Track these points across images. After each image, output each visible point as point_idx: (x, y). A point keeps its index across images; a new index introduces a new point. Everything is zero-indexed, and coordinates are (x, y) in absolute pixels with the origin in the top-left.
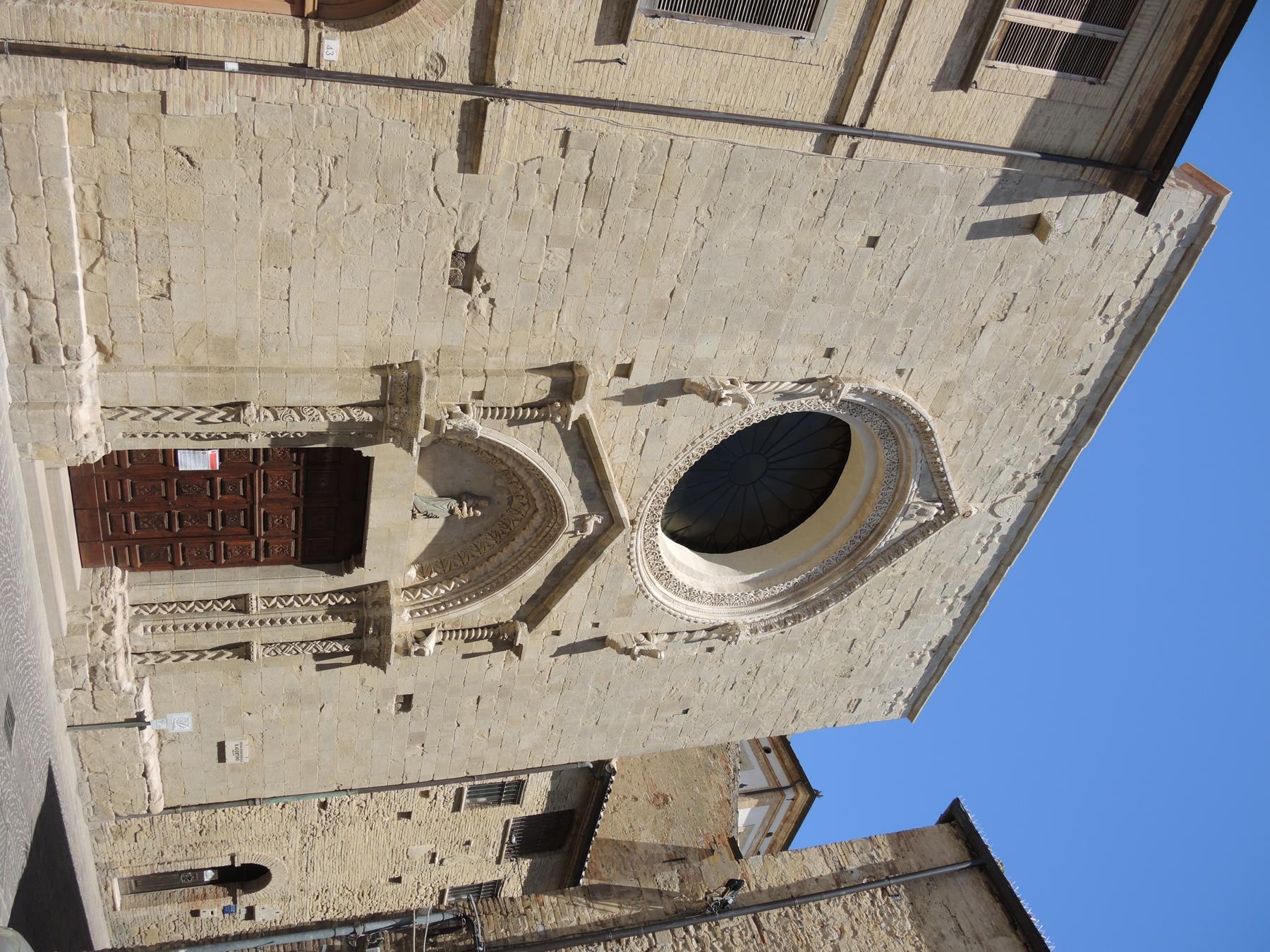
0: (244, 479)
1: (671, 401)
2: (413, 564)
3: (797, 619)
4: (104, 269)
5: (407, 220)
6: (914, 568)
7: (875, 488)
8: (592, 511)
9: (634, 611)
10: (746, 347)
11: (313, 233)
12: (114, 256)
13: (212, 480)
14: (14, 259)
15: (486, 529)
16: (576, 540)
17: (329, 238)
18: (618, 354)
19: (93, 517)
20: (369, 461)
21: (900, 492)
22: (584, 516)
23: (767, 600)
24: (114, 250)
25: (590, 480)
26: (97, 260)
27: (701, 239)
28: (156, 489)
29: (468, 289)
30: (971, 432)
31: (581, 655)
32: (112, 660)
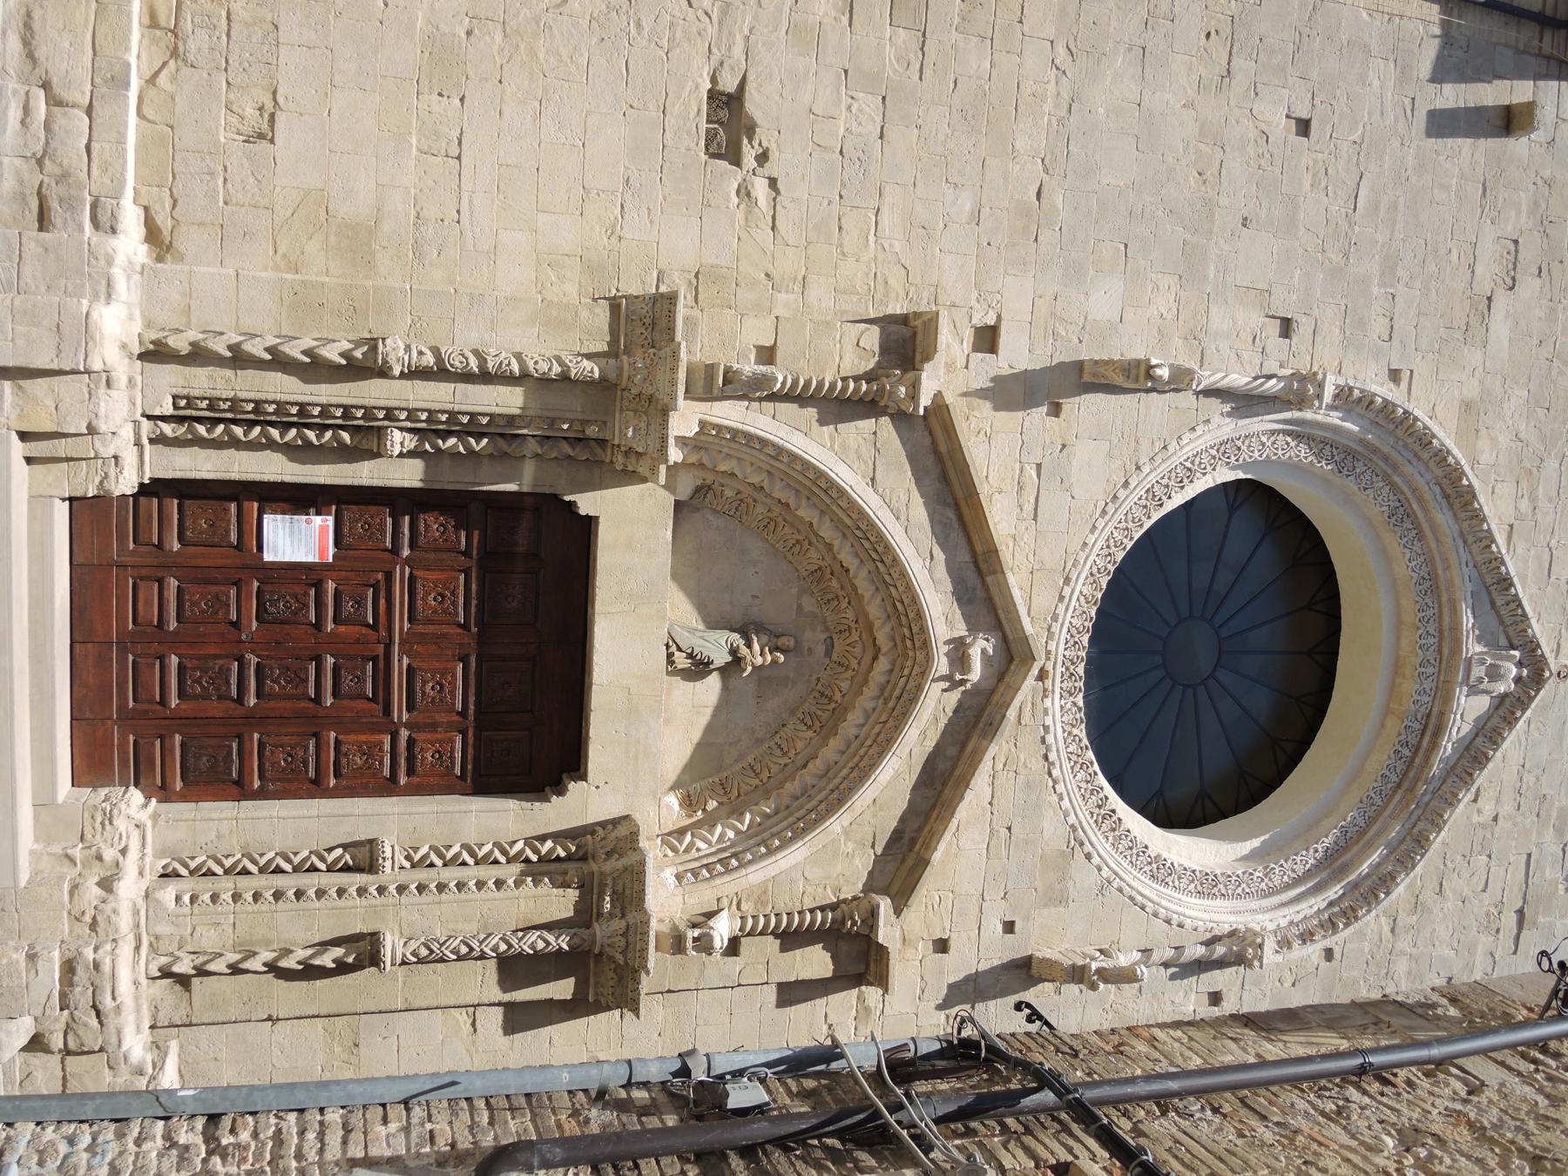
0: (375, 586)
1: (1070, 405)
2: (672, 789)
3: (1350, 915)
4: (173, 79)
5: (639, 25)
6: (1507, 808)
7: (1404, 642)
8: (973, 628)
9: (1073, 894)
10: (1164, 304)
11: (498, 37)
12: (191, 57)
13: (319, 586)
14: (36, 26)
15: (793, 712)
16: (955, 696)
17: (522, 46)
18: (973, 302)
19: (103, 661)
20: (590, 523)
21: (1448, 638)
22: (961, 638)
23: (1288, 887)
24: (192, 45)
25: (964, 556)
26: (165, 64)
27: (1066, 96)
28: (220, 603)
29: (737, 162)
30: (1524, 505)
31: (991, 1003)
32: (108, 947)
